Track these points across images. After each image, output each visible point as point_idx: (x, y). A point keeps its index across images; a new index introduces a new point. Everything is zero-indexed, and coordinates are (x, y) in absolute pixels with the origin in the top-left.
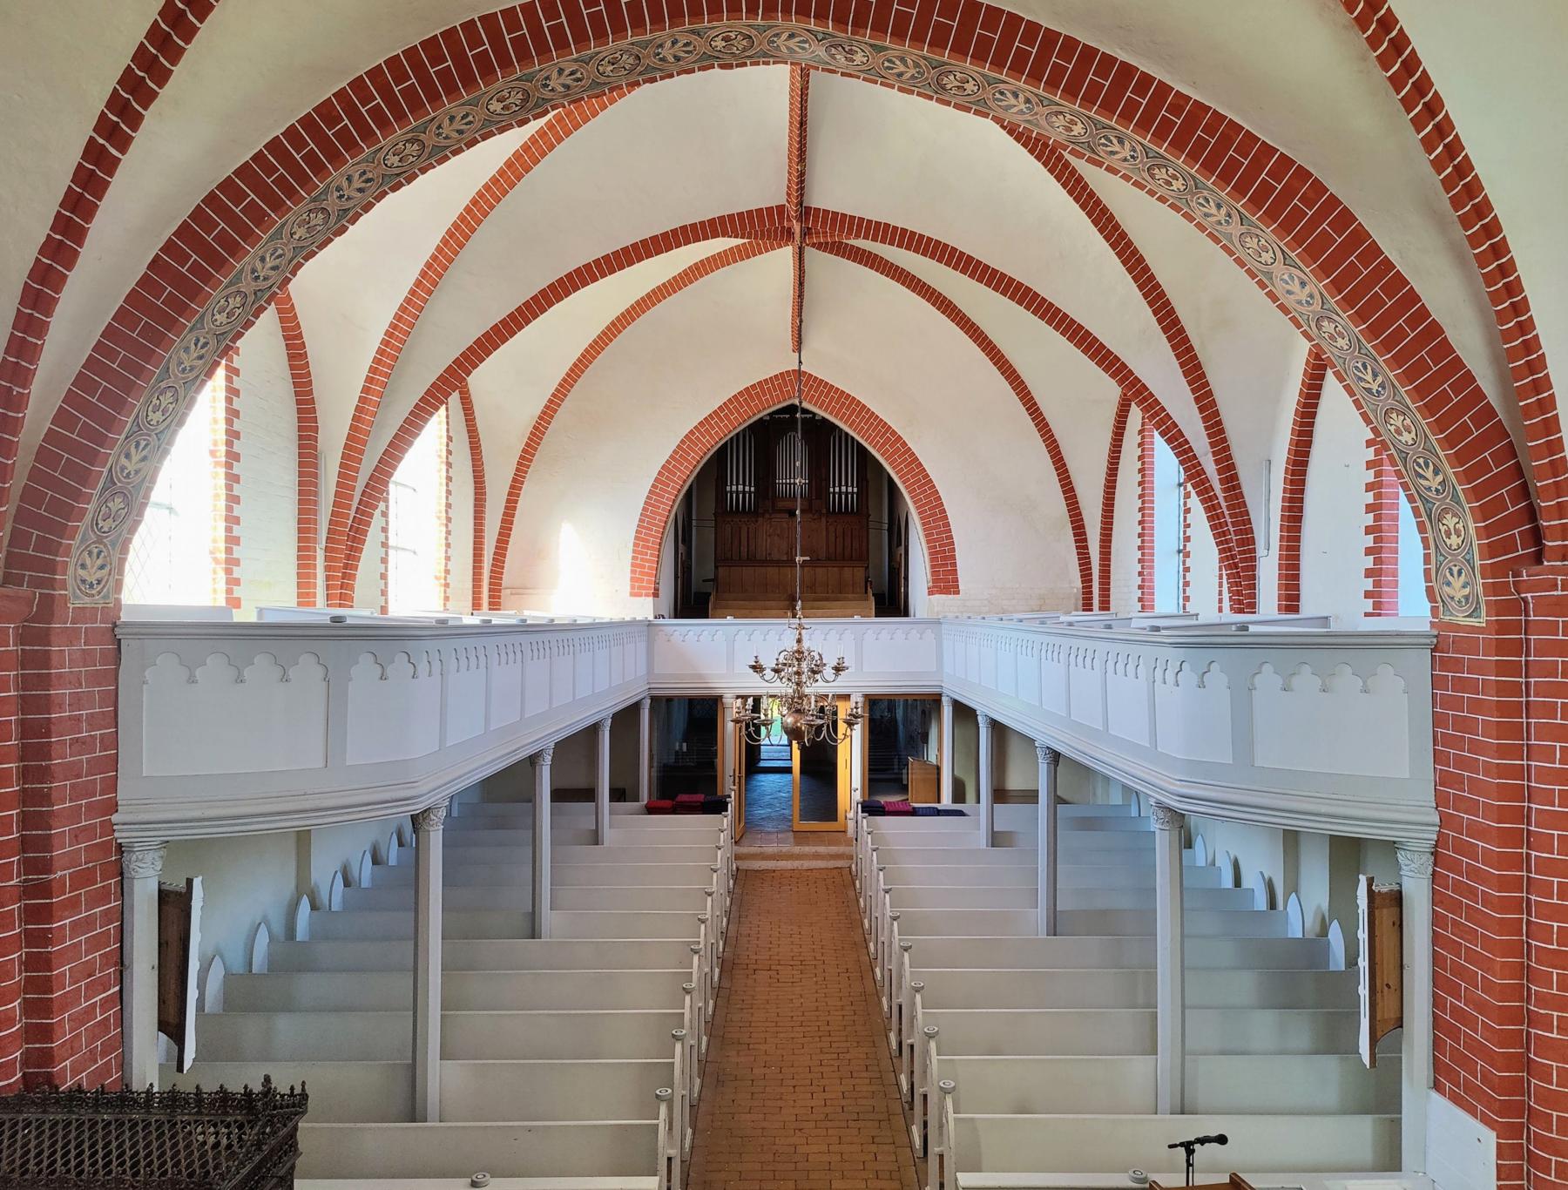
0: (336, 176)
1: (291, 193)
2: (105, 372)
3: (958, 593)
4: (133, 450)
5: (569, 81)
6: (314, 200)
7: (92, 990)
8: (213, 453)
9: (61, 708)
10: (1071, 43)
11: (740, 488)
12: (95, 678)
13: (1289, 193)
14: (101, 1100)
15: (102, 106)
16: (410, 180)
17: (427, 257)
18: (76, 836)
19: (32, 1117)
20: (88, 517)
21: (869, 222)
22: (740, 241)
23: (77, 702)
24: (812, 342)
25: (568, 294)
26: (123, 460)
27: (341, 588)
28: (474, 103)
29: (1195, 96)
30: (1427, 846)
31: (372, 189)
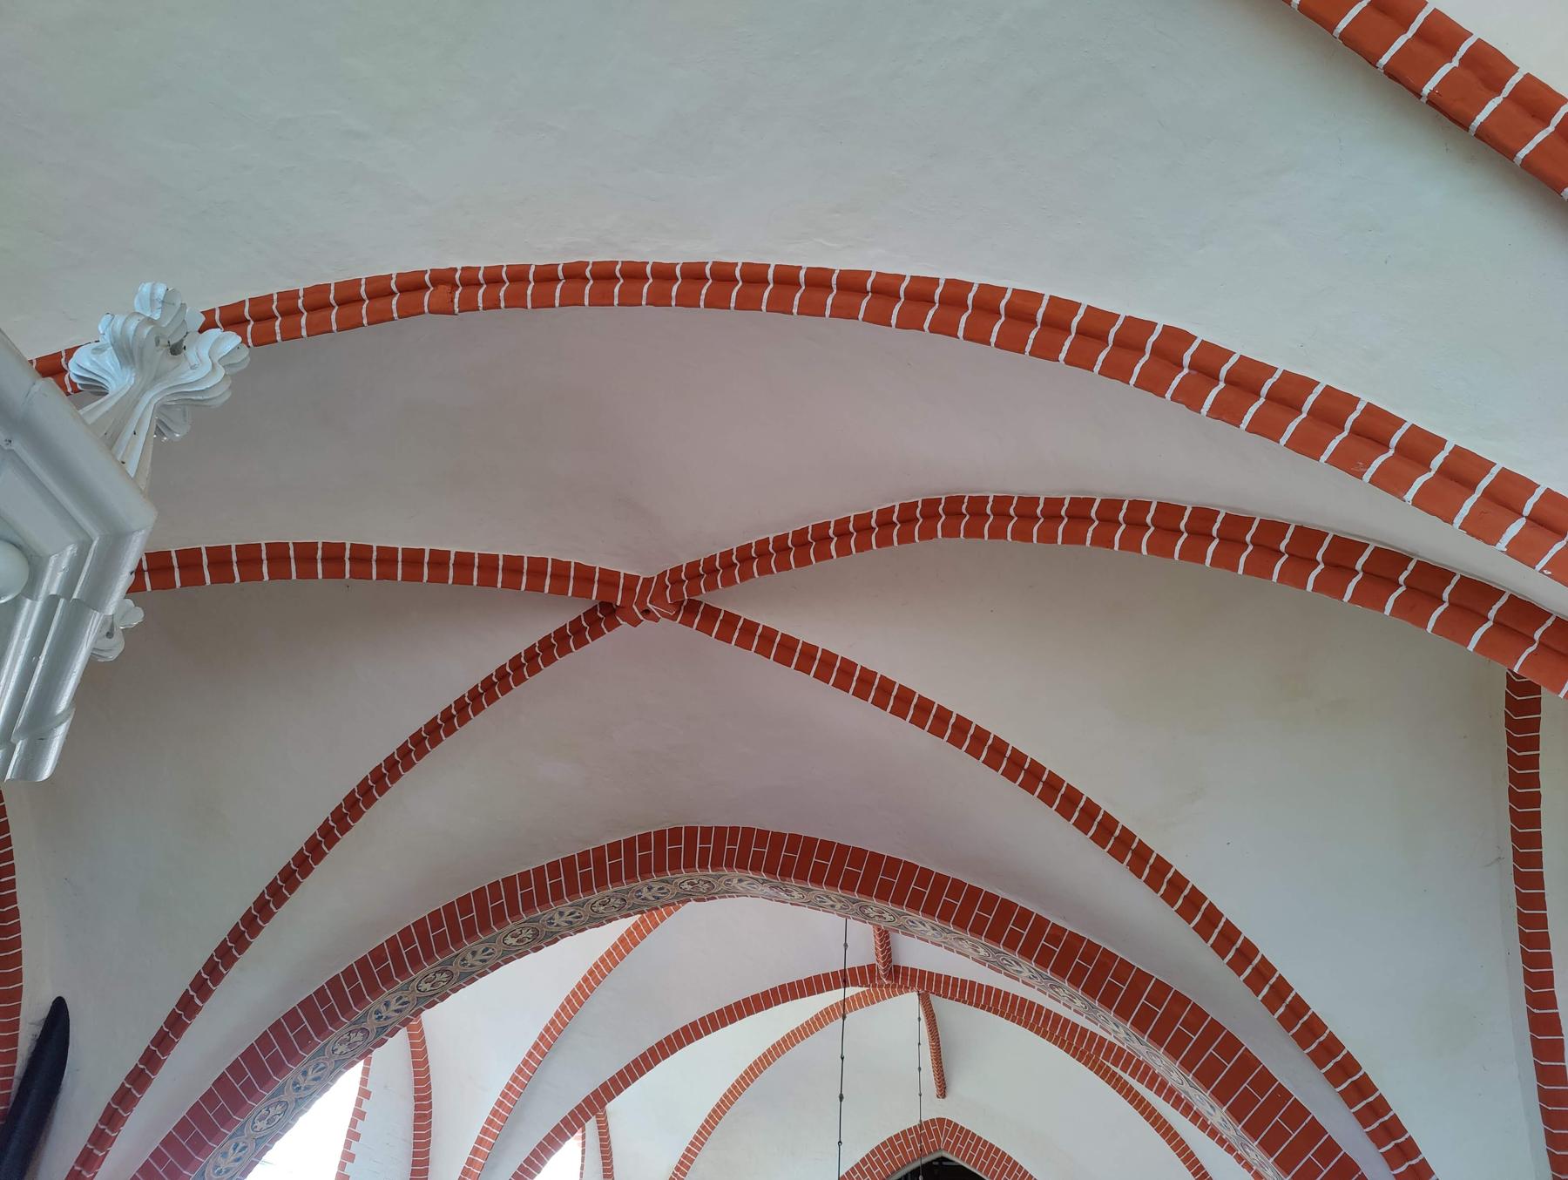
0: (375, 1004)
2: (806, 855)
10: (957, 885)
15: (200, 967)
16: (443, 999)
17: (546, 1022)
21: (956, 979)
22: (858, 990)
24: (957, 1087)
28: (406, 988)
31: (577, 922)
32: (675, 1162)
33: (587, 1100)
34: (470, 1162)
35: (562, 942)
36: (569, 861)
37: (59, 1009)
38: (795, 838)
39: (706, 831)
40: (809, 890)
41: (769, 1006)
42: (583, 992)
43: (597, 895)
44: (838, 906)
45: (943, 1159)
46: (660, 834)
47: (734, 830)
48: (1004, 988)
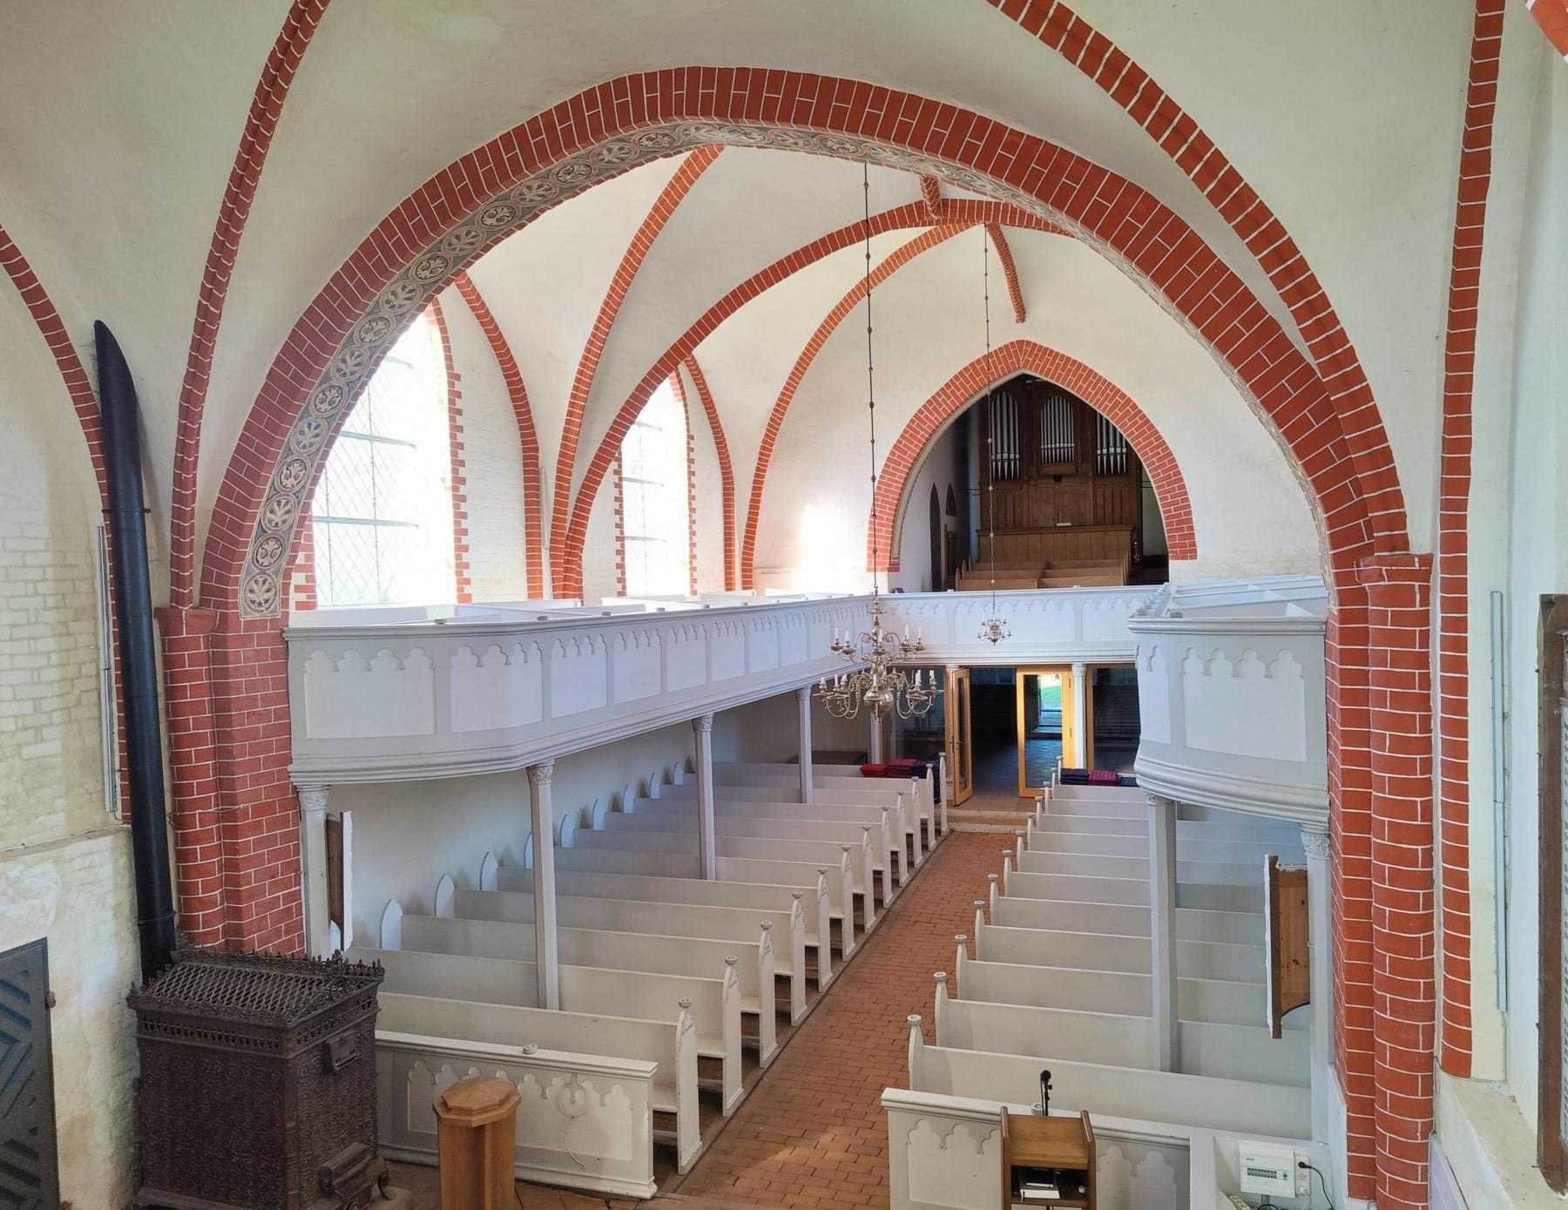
1: (349, 313)
3: (1194, 557)
4: (276, 507)
5: (541, 192)
6: (370, 313)
7: (274, 887)
8: (443, 480)
9: (238, 691)
11: (1005, 453)
12: (267, 670)
13: (1120, 211)
14: (281, 962)
18: (256, 780)
19: (208, 965)
20: (249, 557)
22: (927, 229)
23: (252, 686)
24: (1035, 310)
25: (734, 310)
26: (269, 515)
27: (569, 581)
29: (1027, 132)
30: (1321, 828)
32: (773, 405)
33: (661, 361)
34: (568, 422)
35: (543, 217)
36: (519, 131)
37: (101, 331)
38: (743, 72)
39: (651, 77)
40: (766, 130)
41: (819, 256)
42: (631, 265)
43: (556, 164)
44: (801, 142)
45: (1024, 377)
46: (605, 88)
47: (679, 71)
48: (1214, 213)
